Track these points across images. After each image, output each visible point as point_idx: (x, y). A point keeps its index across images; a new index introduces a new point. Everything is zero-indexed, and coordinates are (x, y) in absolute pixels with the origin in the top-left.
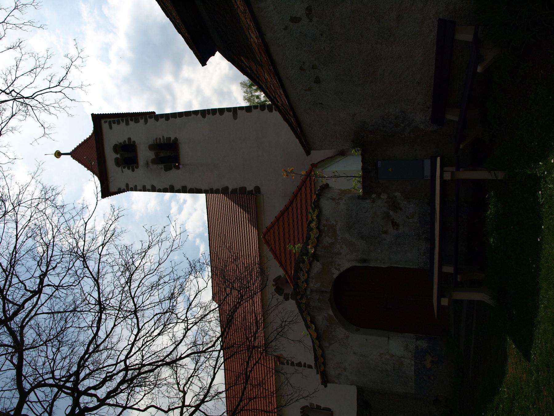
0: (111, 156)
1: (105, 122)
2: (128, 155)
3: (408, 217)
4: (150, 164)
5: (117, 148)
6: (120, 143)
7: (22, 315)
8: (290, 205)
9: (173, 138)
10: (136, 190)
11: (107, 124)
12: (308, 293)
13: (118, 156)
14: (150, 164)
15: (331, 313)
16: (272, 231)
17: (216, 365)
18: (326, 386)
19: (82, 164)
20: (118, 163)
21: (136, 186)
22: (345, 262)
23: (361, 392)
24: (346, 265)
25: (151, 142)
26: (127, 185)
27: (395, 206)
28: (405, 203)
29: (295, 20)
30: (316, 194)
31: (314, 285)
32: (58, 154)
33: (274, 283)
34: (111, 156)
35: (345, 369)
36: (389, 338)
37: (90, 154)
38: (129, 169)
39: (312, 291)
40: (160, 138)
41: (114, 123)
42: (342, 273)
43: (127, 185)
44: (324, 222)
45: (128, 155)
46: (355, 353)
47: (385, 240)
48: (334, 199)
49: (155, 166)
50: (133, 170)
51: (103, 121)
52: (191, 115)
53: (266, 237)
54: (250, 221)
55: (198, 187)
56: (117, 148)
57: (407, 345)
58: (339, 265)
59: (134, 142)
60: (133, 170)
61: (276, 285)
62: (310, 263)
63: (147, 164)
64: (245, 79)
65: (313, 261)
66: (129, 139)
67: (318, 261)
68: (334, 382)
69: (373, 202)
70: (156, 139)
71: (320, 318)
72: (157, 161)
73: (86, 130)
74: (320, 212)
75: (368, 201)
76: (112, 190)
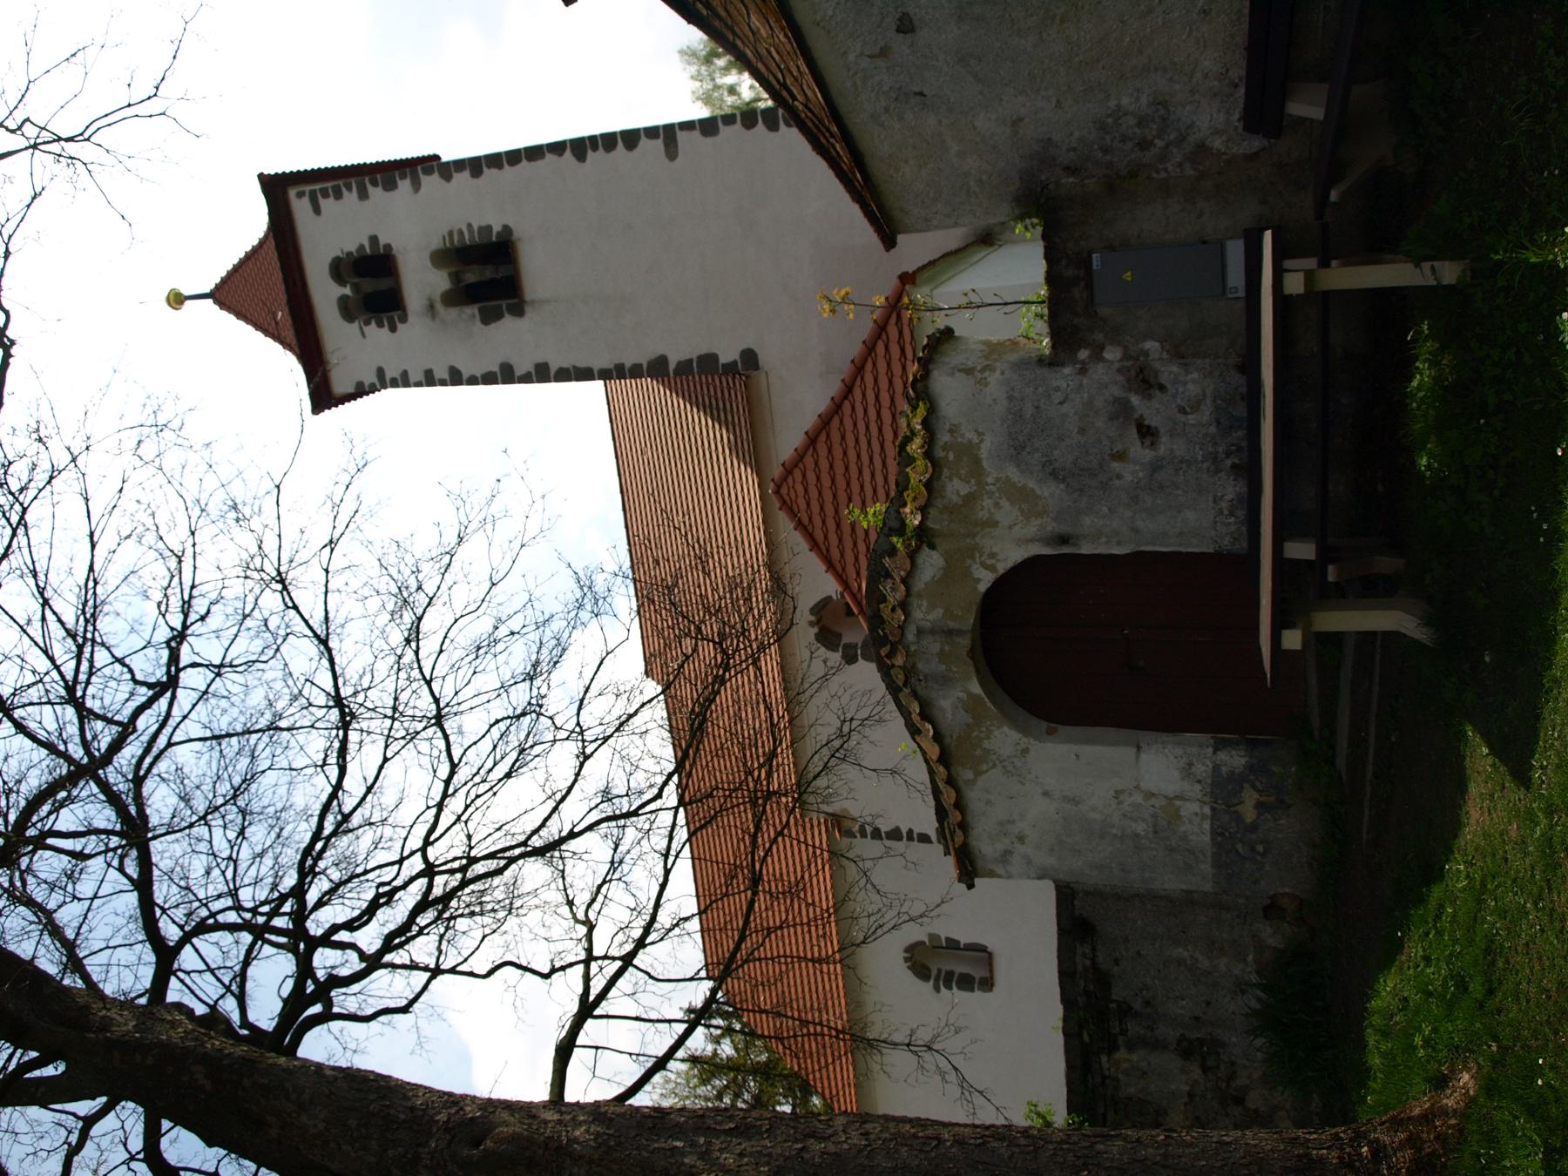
1: (300, 195)
2: (374, 284)
3: (1182, 410)
4: (439, 307)
5: (340, 269)
6: (349, 254)
8: (846, 397)
9: (497, 228)
10: (406, 384)
11: (306, 200)
12: (910, 636)
13: (347, 291)
14: (439, 307)
15: (976, 688)
18: (971, 886)
20: (347, 310)
21: (405, 374)
22: (1010, 544)
23: (1066, 896)
24: (1011, 555)
25: (436, 243)
26: (380, 373)
27: (1144, 380)
28: (1175, 369)
30: (919, 360)
31: (924, 614)
32: (177, 300)
33: (813, 618)
34: (326, 294)
35: (1021, 839)
36: (1139, 748)
38: (380, 325)
39: (920, 632)
40: (461, 232)
42: (1003, 576)
43: (380, 373)
44: (944, 437)
45: (374, 284)
46: (1046, 794)
47: (1119, 477)
48: (969, 371)
49: (453, 312)
50: (393, 329)
51: (292, 193)
53: (784, 491)
54: (735, 449)
55: (582, 364)
56: (340, 269)
57: (1190, 764)
58: (993, 555)
59: (388, 247)
60: (393, 329)
61: (819, 622)
62: (912, 556)
65: (918, 548)
66: (374, 240)
67: (932, 547)
69: (1083, 371)
70: (451, 233)
71: (948, 705)
72: (461, 295)
74: (932, 409)
75: (1067, 370)
76: (340, 385)
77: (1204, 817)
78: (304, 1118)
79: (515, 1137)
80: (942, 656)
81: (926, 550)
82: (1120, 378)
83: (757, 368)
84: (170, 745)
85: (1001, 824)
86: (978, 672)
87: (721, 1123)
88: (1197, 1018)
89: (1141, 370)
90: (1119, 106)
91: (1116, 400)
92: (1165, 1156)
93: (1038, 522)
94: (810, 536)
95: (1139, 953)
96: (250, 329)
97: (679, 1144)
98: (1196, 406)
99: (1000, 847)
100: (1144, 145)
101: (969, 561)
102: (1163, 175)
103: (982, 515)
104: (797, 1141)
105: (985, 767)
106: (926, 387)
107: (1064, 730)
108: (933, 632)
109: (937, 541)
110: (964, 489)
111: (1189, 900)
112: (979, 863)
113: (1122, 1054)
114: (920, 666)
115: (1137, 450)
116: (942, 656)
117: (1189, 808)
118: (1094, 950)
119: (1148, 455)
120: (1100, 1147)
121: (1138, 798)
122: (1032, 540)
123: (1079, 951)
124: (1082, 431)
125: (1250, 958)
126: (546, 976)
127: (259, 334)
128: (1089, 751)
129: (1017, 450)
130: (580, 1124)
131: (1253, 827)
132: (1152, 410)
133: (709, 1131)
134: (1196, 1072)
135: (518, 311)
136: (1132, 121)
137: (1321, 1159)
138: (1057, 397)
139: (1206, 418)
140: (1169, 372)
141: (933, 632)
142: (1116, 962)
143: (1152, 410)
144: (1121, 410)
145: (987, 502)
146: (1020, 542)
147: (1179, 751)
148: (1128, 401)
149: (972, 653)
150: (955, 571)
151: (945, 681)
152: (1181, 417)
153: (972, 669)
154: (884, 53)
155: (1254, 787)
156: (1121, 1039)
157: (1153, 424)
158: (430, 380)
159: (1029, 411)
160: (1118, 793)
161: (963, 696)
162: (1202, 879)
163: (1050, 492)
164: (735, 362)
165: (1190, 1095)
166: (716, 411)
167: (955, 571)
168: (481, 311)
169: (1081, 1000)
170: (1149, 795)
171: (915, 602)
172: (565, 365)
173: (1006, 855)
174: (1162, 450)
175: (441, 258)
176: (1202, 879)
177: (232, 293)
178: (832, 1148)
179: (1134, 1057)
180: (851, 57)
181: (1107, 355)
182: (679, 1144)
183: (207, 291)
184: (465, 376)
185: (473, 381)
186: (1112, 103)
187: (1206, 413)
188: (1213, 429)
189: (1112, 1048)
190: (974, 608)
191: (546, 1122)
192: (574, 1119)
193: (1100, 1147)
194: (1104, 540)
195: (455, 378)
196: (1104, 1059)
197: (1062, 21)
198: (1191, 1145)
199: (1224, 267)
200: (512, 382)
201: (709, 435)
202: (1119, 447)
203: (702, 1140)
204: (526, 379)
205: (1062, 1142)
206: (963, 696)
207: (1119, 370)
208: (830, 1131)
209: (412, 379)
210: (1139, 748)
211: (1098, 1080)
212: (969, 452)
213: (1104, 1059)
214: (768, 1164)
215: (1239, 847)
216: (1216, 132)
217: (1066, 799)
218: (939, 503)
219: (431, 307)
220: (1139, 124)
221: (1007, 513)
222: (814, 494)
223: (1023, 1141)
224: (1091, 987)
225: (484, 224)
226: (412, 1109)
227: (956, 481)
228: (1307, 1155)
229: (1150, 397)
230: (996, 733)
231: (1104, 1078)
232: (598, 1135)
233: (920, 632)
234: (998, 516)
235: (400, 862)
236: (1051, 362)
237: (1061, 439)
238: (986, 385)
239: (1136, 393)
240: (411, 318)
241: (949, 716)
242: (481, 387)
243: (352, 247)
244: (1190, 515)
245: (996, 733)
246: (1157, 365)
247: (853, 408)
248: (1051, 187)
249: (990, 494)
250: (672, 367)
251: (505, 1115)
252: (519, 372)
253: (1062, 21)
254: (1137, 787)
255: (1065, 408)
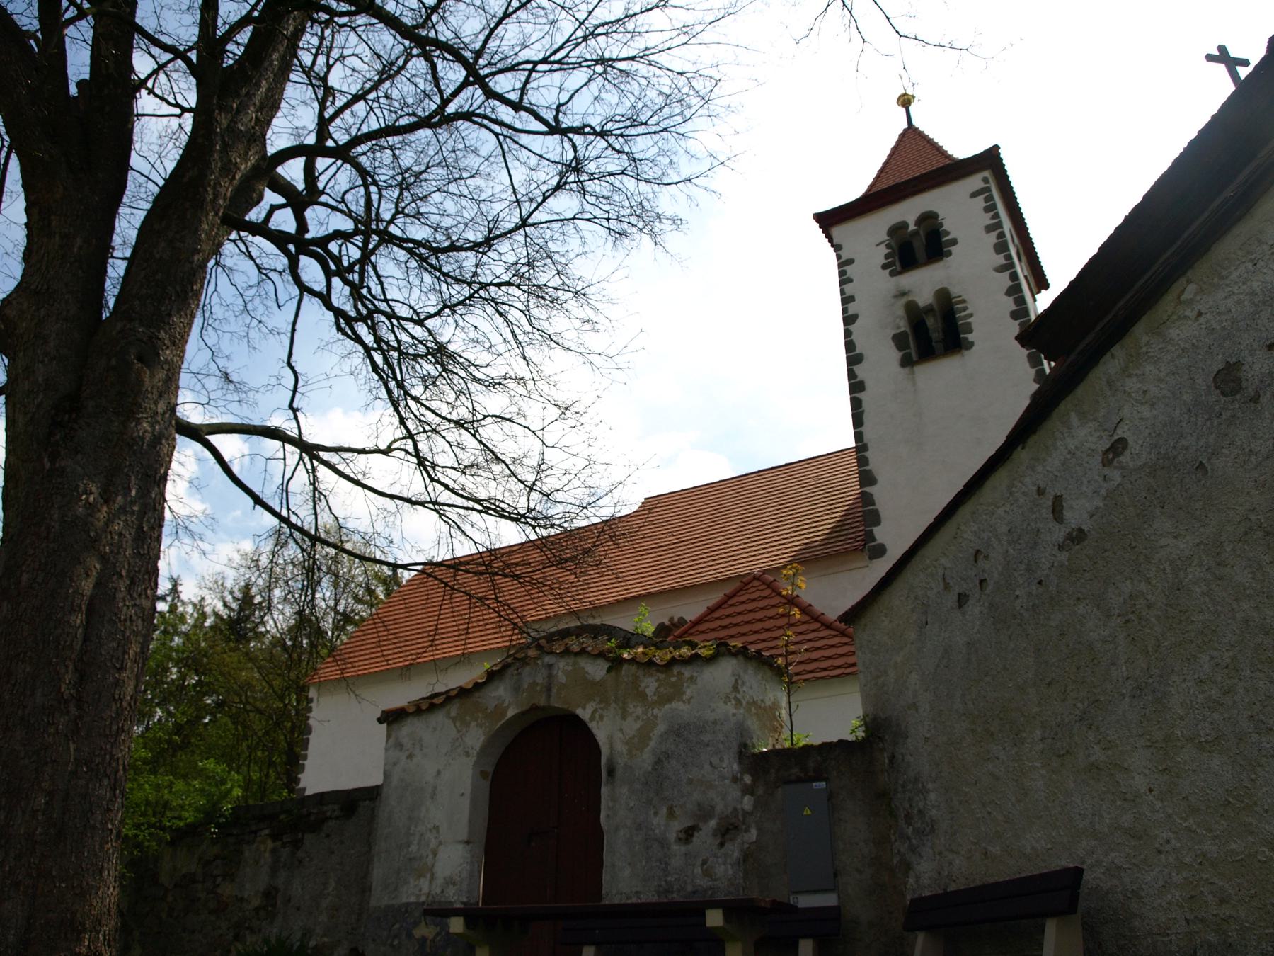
0: (908, 212)
1: (986, 180)
2: (919, 247)
3: (704, 862)
4: (904, 300)
5: (929, 221)
6: (941, 225)
7: (505, 113)
8: (823, 624)
9: (970, 337)
10: (842, 283)
11: (982, 185)
12: (547, 659)
13: (912, 227)
14: (904, 300)
15: (511, 713)
16: (768, 592)
17: (440, 504)
18: (380, 721)
19: (890, 157)
20: (897, 230)
21: (850, 280)
22: (608, 731)
23: (372, 794)
24: (601, 733)
25: (955, 291)
26: (850, 262)
27: (727, 830)
28: (736, 854)
29: (1057, 509)
30: (745, 648)
31: (563, 667)
32: (905, 101)
33: (676, 620)
34: (908, 212)
35: (410, 757)
36: (467, 842)
37: (917, 168)
38: (887, 256)
39: (550, 666)
40: (965, 309)
41: (986, 200)
42: (586, 726)
43: (850, 262)
44: (687, 672)
45: (919, 247)
46: (439, 772)
47: (656, 814)
48: (735, 688)
49: (900, 312)
50: (884, 267)
51: (987, 174)
52: (1033, 366)
53: (756, 583)
54: (808, 547)
55: (866, 418)
56: (929, 221)
57: (454, 884)
58: (601, 717)
59: (949, 253)
60: (884, 267)
61: (673, 625)
62: (601, 655)
63: (903, 294)
64: (1019, 448)
65: (607, 659)
66: (954, 242)
67: (609, 670)
68: (389, 736)
69: (735, 780)
70: (964, 301)
71: (500, 692)
72: (916, 316)
73: (961, 147)
74: (710, 660)
75: (735, 766)
76: (836, 231)
77: (418, 896)
78: (163, 244)
79: (140, 382)
80: (534, 684)
81: (606, 665)
82: (730, 810)
83: (871, 558)
84: (497, 135)
85: (421, 740)
86: (523, 714)
87: (148, 521)
88: (289, 901)
89: (736, 828)
90: (928, 791)
91: (713, 807)
92: (94, 827)
93: (625, 751)
94: (719, 606)
95: (333, 853)
96: (884, 158)
97: (133, 493)
98: (707, 873)
99: (405, 741)
100: (908, 817)
101: (598, 699)
102: (893, 838)
103: (631, 708)
104: (128, 572)
105: (458, 724)
106: (723, 655)
107: (486, 785)
108: (550, 676)
109: (613, 674)
110: (649, 692)
111: (365, 890)
112: (395, 726)
113: (270, 844)
114: (528, 668)
115: (677, 826)
116: (534, 684)
117: (424, 884)
118: (337, 818)
119: (672, 836)
120: (106, 782)
121: (433, 844)
122: (611, 748)
123: (336, 807)
124: (690, 782)
125: (326, 940)
126: (291, 407)
127: (879, 166)
128: (466, 804)
129: (678, 731)
130: (152, 426)
131: (410, 936)
132: (705, 837)
133: (143, 513)
134: (256, 902)
135: (906, 362)
136: (921, 805)
137: (80, 940)
138: (715, 760)
139: (698, 882)
140: (734, 850)
141: (550, 676)
142: (328, 836)
143: (705, 837)
144: (704, 813)
145: (639, 710)
146: (610, 739)
147: (465, 874)
148: (711, 817)
149: (534, 708)
150: (594, 690)
151: (517, 689)
152: (699, 862)
153: (524, 708)
154: (947, 587)
155: (437, 934)
156: (279, 843)
157: (694, 839)
158: (846, 300)
159: (706, 738)
160: (436, 828)
161: (506, 704)
162: (379, 899)
163: (646, 759)
164: (874, 540)
165: (242, 899)
166: (839, 530)
167: (594, 690)
168: (904, 334)
169: (305, 811)
170: (435, 854)
171: (571, 660)
172: (864, 404)
173: (399, 746)
174: (675, 847)
175: (944, 296)
176: (379, 899)
177: (912, 139)
178: (119, 595)
179: (267, 855)
180: (943, 561)
181: (747, 799)
182: (133, 493)
183: (914, 122)
184: (851, 327)
185: (847, 334)
186: (930, 786)
187: (703, 882)
188: (690, 888)
189: (275, 837)
190: (565, 707)
191: (156, 403)
192: (158, 422)
193: (106, 782)
194: (611, 804)
195: (849, 320)
196: (267, 832)
197: (973, 731)
198: (102, 847)
199: (815, 892)
200: (848, 364)
201: (818, 530)
202: (678, 811)
203: (136, 508)
204: (851, 375)
205: (112, 756)
206: (506, 704)
207: (735, 809)
208: (135, 595)
209: (846, 287)
210: (467, 842)
211: (254, 828)
212: (676, 693)
213: (267, 832)
214: (112, 552)
215: (397, 926)
216: (918, 878)
217: (435, 788)
218: (640, 673)
219: (903, 294)
220: (920, 811)
221: (632, 726)
222: (750, 606)
223: (114, 728)
224: (312, 818)
225: (974, 327)
226: (170, 315)
227: (656, 684)
228: (84, 931)
229: (715, 835)
230: (481, 731)
231: (255, 832)
232: (142, 438)
233: (550, 666)
234: (629, 719)
235: (386, 300)
236: (745, 754)
237: (685, 765)
238: (726, 703)
239: (718, 824)
240: (894, 279)
241: (493, 694)
242: (843, 341)
243: (946, 227)
244: (627, 872)
245: (481, 731)
246: (739, 840)
247: (814, 631)
248: (881, 745)
249: (645, 713)
250: (868, 489)
251: (161, 375)
252: (856, 369)
253: (973, 731)
254: (440, 843)
255: (707, 766)
